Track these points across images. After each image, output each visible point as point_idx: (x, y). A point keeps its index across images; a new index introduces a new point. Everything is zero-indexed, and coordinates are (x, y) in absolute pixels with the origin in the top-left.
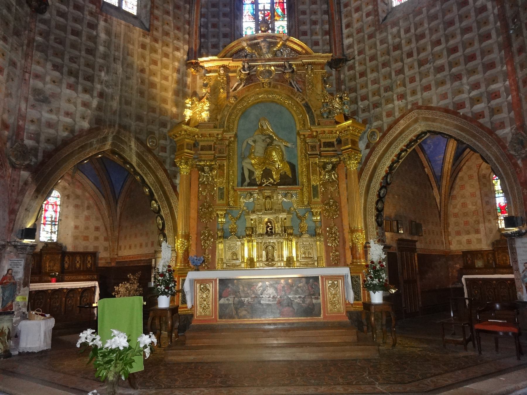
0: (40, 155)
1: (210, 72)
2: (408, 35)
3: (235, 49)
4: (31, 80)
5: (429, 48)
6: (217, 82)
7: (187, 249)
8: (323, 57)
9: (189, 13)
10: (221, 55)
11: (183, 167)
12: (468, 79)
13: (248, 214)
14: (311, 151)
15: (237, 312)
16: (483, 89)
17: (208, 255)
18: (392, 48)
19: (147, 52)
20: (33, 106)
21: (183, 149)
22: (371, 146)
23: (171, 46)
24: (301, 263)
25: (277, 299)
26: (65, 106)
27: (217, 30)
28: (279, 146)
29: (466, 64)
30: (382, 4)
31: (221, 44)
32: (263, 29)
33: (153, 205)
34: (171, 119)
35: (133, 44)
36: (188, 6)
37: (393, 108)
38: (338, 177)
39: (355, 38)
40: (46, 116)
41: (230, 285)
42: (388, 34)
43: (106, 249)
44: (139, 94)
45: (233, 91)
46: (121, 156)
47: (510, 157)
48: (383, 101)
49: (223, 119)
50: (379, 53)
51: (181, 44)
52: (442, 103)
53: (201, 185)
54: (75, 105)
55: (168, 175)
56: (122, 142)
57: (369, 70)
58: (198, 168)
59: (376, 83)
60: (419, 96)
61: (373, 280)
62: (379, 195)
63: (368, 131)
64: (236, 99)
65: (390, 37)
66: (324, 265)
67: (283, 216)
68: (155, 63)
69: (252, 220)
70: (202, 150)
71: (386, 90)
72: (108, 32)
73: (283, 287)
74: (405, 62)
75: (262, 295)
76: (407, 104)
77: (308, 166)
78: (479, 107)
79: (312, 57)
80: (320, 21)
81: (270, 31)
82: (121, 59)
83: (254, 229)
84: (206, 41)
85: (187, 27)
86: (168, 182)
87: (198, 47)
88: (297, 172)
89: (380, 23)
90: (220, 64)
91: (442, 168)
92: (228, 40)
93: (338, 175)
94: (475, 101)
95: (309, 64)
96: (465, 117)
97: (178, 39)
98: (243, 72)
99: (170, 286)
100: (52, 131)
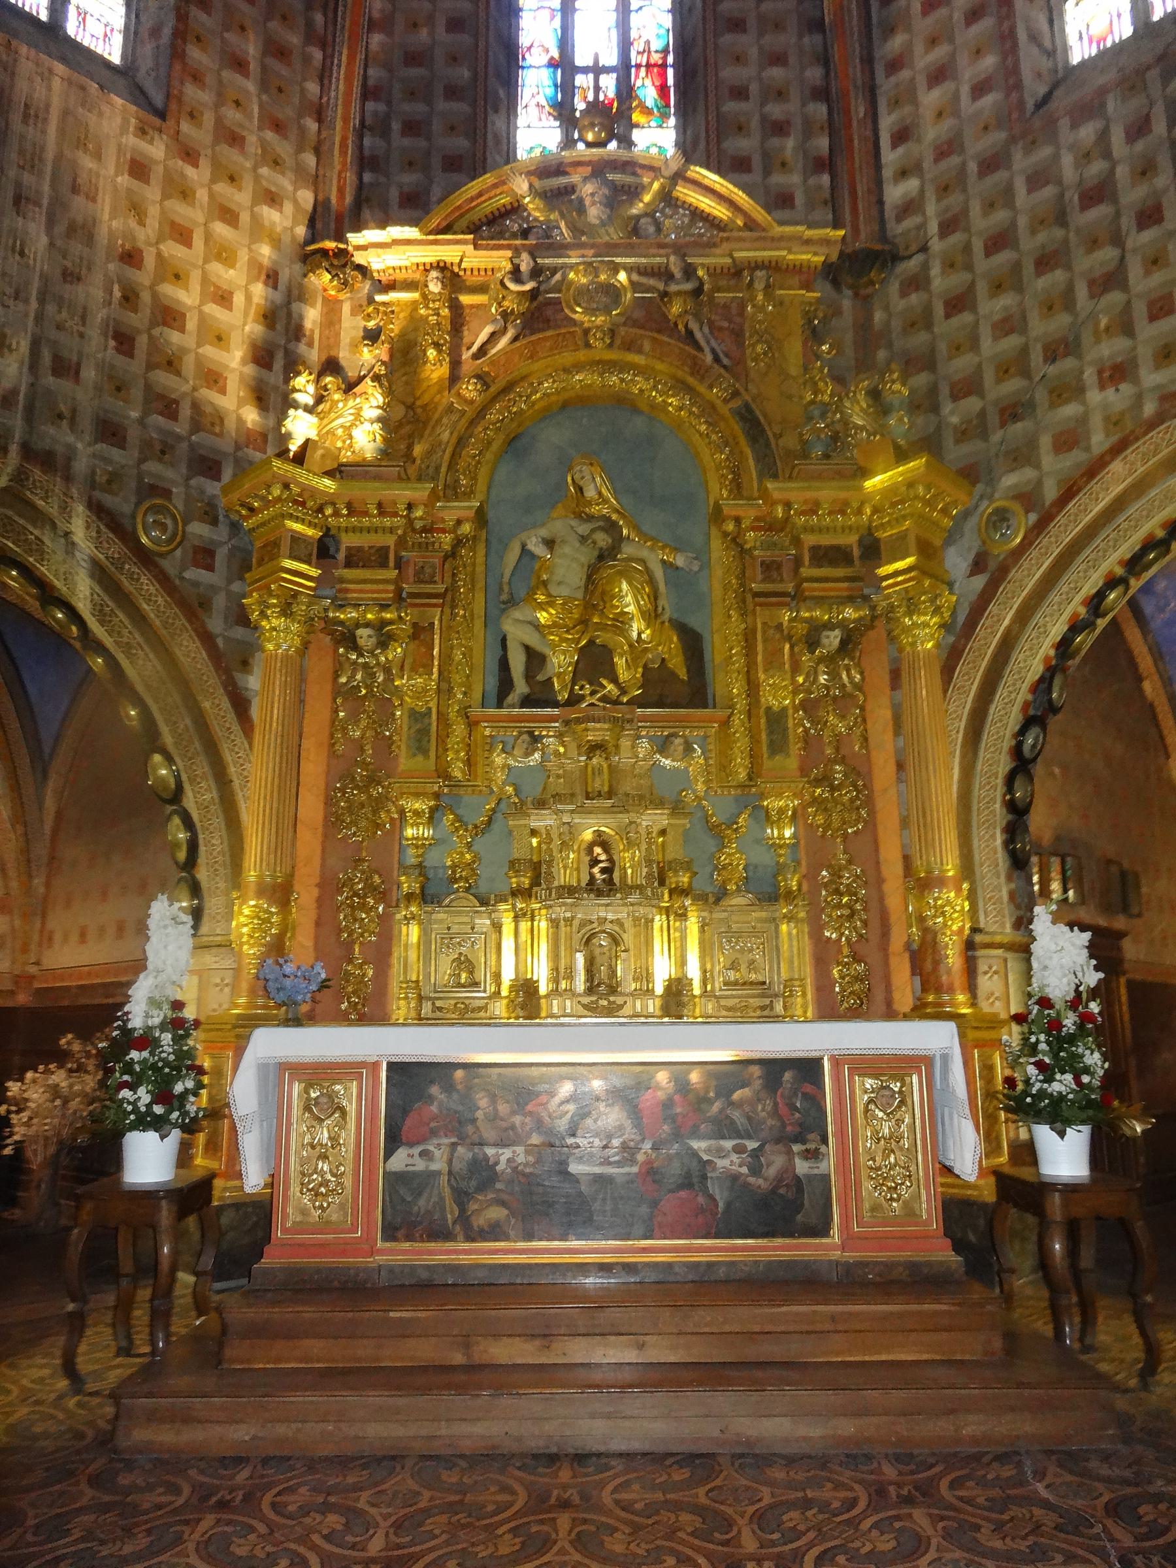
1: (391, 286)
2: (1140, 146)
6: (415, 324)
8: (808, 242)
9: (321, 79)
10: (434, 223)
11: (275, 622)
13: (520, 809)
14: (763, 581)
15: (463, 1210)
17: (361, 966)
18: (1076, 197)
19: (152, 193)
21: (274, 557)
22: (992, 565)
23: (248, 182)
24: (723, 1002)
25: (640, 1157)
27: (422, 143)
28: (642, 561)
30: (1035, 50)
32: (590, 137)
33: (155, 770)
34: (238, 447)
35: (98, 156)
36: (317, 55)
37: (1083, 420)
38: (863, 679)
39: (928, 176)
41: (435, 1090)
42: (1058, 147)
44: (112, 343)
46: (27, 573)
48: (1041, 395)
49: (434, 457)
50: (1022, 222)
51: (285, 182)
53: (345, 700)
55: (215, 655)
57: (982, 288)
58: (332, 633)
59: (1011, 331)
61: (1049, 1080)
62: (1017, 751)
63: (982, 508)
65: (1067, 160)
66: (809, 1014)
67: (653, 819)
68: (183, 236)
69: (534, 833)
70: (349, 564)
71: (1051, 356)
73: (668, 1104)
74: (1130, 244)
75: (574, 1135)
76: (1139, 399)
77: (749, 638)
79: (773, 239)
80: (798, 121)
81: (613, 145)
82: (45, 202)
83: (544, 867)
84: (382, 179)
85: (312, 125)
87: (348, 199)
88: (707, 656)
89: (1028, 114)
90: (428, 260)
93: (862, 673)
95: (756, 266)
97: (276, 163)
98: (513, 286)
99: (179, 1088)
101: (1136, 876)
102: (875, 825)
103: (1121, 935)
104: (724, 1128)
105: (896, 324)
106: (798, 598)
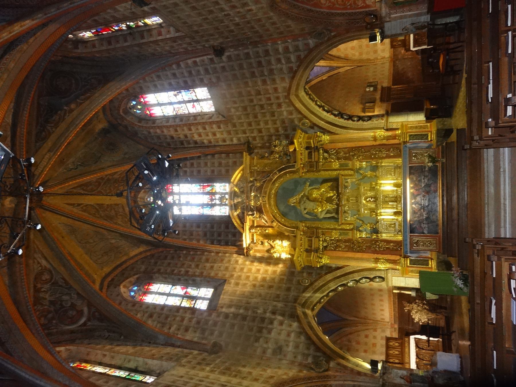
0: (318, 354)
1: (253, 239)
3: (238, 220)
4: (267, 356)
5: (249, 89)
7: (386, 260)
12: (273, 65)
16: (281, 56)
19: (241, 282)
20: (285, 356)
25: (425, 194)
26: (283, 336)
27: (223, 233)
29: (263, 67)
30: (213, 118)
31: (233, 230)
35: (236, 291)
37: (287, 111)
40: (290, 348)
43: (383, 331)
45: (267, 223)
47: (328, 40)
48: (281, 117)
52: (287, 80)
54: (281, 330)
56: (305, 302)
60: (280, 95)
62: (348, 119)
64: (274, 221)
65: (237, 113)
70: (311, 247)
72: (230, 306)
73: (416, 190)
76: (285, 102)
78: (293, 58)
84: (230, 241)
85: (220, 254)
86: (334, 273)
87: (235, 247)
91: (323, 66)
92: (230, 225)
94: (288, 60)
96: (299, 67)
100: (301, 346)
101: (369, 83)
102: (363, 146)
103: (382, 87)
104: (420, 181)
105: (262, 142)
106: (317, 162)
